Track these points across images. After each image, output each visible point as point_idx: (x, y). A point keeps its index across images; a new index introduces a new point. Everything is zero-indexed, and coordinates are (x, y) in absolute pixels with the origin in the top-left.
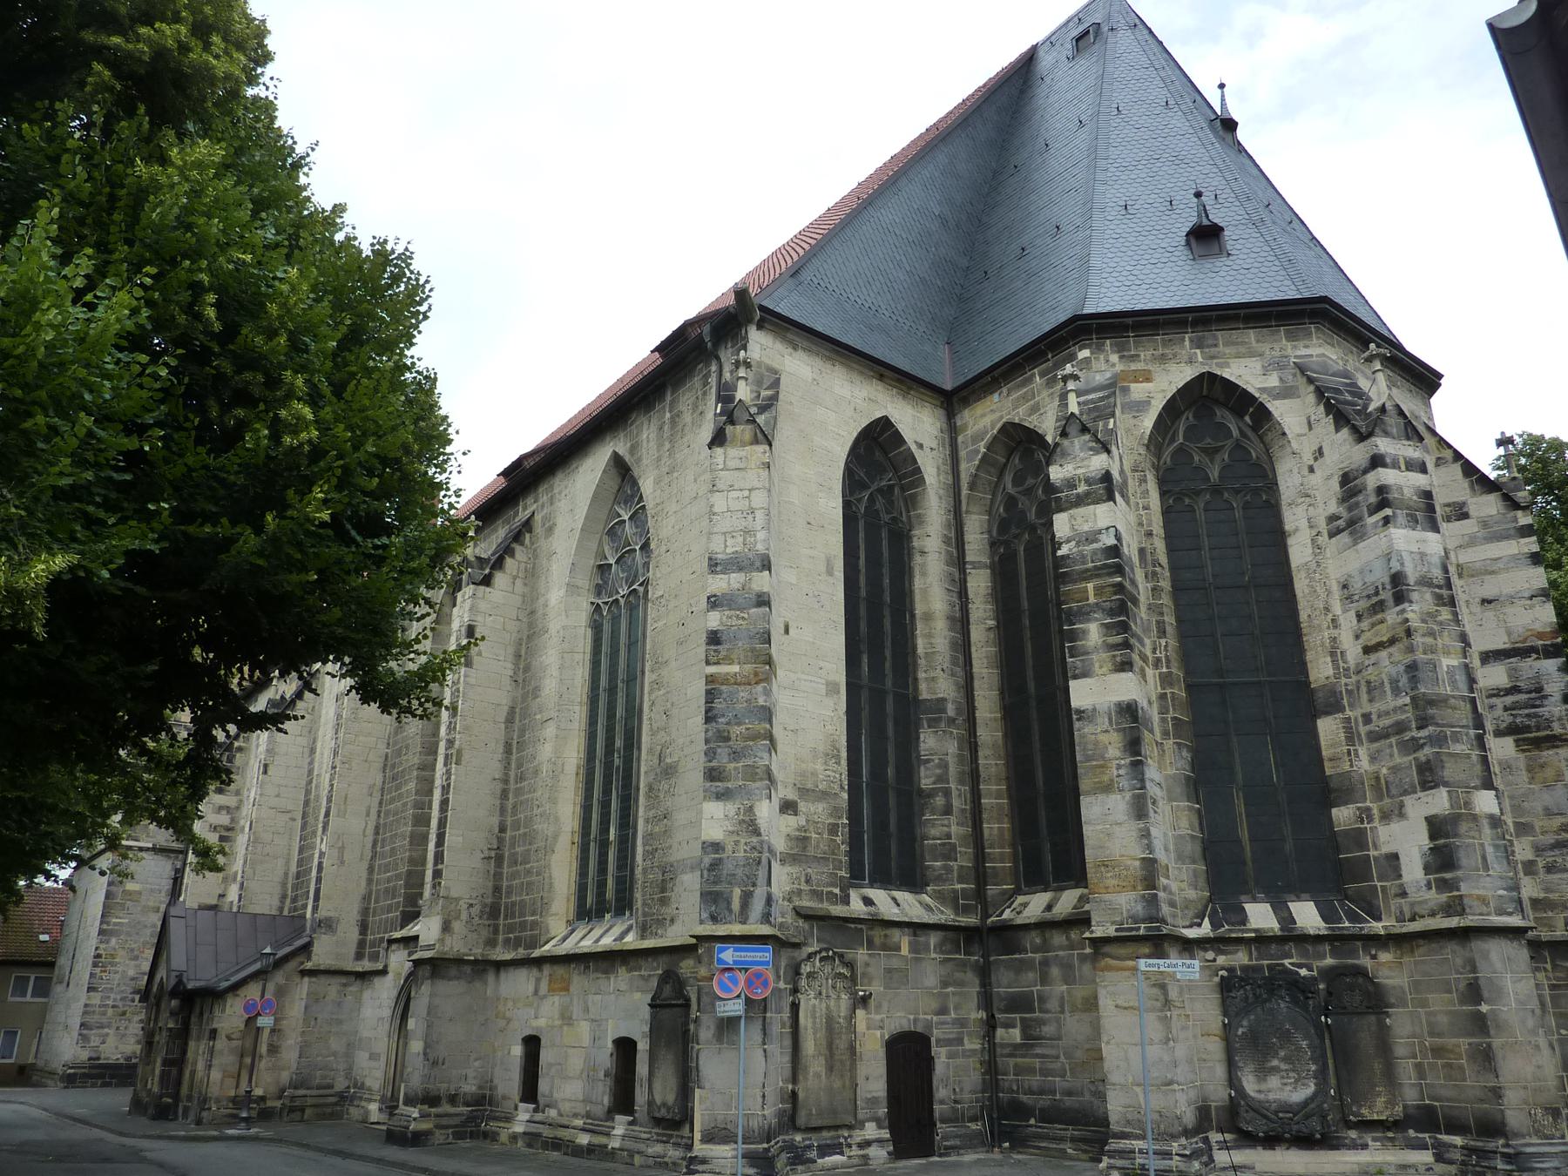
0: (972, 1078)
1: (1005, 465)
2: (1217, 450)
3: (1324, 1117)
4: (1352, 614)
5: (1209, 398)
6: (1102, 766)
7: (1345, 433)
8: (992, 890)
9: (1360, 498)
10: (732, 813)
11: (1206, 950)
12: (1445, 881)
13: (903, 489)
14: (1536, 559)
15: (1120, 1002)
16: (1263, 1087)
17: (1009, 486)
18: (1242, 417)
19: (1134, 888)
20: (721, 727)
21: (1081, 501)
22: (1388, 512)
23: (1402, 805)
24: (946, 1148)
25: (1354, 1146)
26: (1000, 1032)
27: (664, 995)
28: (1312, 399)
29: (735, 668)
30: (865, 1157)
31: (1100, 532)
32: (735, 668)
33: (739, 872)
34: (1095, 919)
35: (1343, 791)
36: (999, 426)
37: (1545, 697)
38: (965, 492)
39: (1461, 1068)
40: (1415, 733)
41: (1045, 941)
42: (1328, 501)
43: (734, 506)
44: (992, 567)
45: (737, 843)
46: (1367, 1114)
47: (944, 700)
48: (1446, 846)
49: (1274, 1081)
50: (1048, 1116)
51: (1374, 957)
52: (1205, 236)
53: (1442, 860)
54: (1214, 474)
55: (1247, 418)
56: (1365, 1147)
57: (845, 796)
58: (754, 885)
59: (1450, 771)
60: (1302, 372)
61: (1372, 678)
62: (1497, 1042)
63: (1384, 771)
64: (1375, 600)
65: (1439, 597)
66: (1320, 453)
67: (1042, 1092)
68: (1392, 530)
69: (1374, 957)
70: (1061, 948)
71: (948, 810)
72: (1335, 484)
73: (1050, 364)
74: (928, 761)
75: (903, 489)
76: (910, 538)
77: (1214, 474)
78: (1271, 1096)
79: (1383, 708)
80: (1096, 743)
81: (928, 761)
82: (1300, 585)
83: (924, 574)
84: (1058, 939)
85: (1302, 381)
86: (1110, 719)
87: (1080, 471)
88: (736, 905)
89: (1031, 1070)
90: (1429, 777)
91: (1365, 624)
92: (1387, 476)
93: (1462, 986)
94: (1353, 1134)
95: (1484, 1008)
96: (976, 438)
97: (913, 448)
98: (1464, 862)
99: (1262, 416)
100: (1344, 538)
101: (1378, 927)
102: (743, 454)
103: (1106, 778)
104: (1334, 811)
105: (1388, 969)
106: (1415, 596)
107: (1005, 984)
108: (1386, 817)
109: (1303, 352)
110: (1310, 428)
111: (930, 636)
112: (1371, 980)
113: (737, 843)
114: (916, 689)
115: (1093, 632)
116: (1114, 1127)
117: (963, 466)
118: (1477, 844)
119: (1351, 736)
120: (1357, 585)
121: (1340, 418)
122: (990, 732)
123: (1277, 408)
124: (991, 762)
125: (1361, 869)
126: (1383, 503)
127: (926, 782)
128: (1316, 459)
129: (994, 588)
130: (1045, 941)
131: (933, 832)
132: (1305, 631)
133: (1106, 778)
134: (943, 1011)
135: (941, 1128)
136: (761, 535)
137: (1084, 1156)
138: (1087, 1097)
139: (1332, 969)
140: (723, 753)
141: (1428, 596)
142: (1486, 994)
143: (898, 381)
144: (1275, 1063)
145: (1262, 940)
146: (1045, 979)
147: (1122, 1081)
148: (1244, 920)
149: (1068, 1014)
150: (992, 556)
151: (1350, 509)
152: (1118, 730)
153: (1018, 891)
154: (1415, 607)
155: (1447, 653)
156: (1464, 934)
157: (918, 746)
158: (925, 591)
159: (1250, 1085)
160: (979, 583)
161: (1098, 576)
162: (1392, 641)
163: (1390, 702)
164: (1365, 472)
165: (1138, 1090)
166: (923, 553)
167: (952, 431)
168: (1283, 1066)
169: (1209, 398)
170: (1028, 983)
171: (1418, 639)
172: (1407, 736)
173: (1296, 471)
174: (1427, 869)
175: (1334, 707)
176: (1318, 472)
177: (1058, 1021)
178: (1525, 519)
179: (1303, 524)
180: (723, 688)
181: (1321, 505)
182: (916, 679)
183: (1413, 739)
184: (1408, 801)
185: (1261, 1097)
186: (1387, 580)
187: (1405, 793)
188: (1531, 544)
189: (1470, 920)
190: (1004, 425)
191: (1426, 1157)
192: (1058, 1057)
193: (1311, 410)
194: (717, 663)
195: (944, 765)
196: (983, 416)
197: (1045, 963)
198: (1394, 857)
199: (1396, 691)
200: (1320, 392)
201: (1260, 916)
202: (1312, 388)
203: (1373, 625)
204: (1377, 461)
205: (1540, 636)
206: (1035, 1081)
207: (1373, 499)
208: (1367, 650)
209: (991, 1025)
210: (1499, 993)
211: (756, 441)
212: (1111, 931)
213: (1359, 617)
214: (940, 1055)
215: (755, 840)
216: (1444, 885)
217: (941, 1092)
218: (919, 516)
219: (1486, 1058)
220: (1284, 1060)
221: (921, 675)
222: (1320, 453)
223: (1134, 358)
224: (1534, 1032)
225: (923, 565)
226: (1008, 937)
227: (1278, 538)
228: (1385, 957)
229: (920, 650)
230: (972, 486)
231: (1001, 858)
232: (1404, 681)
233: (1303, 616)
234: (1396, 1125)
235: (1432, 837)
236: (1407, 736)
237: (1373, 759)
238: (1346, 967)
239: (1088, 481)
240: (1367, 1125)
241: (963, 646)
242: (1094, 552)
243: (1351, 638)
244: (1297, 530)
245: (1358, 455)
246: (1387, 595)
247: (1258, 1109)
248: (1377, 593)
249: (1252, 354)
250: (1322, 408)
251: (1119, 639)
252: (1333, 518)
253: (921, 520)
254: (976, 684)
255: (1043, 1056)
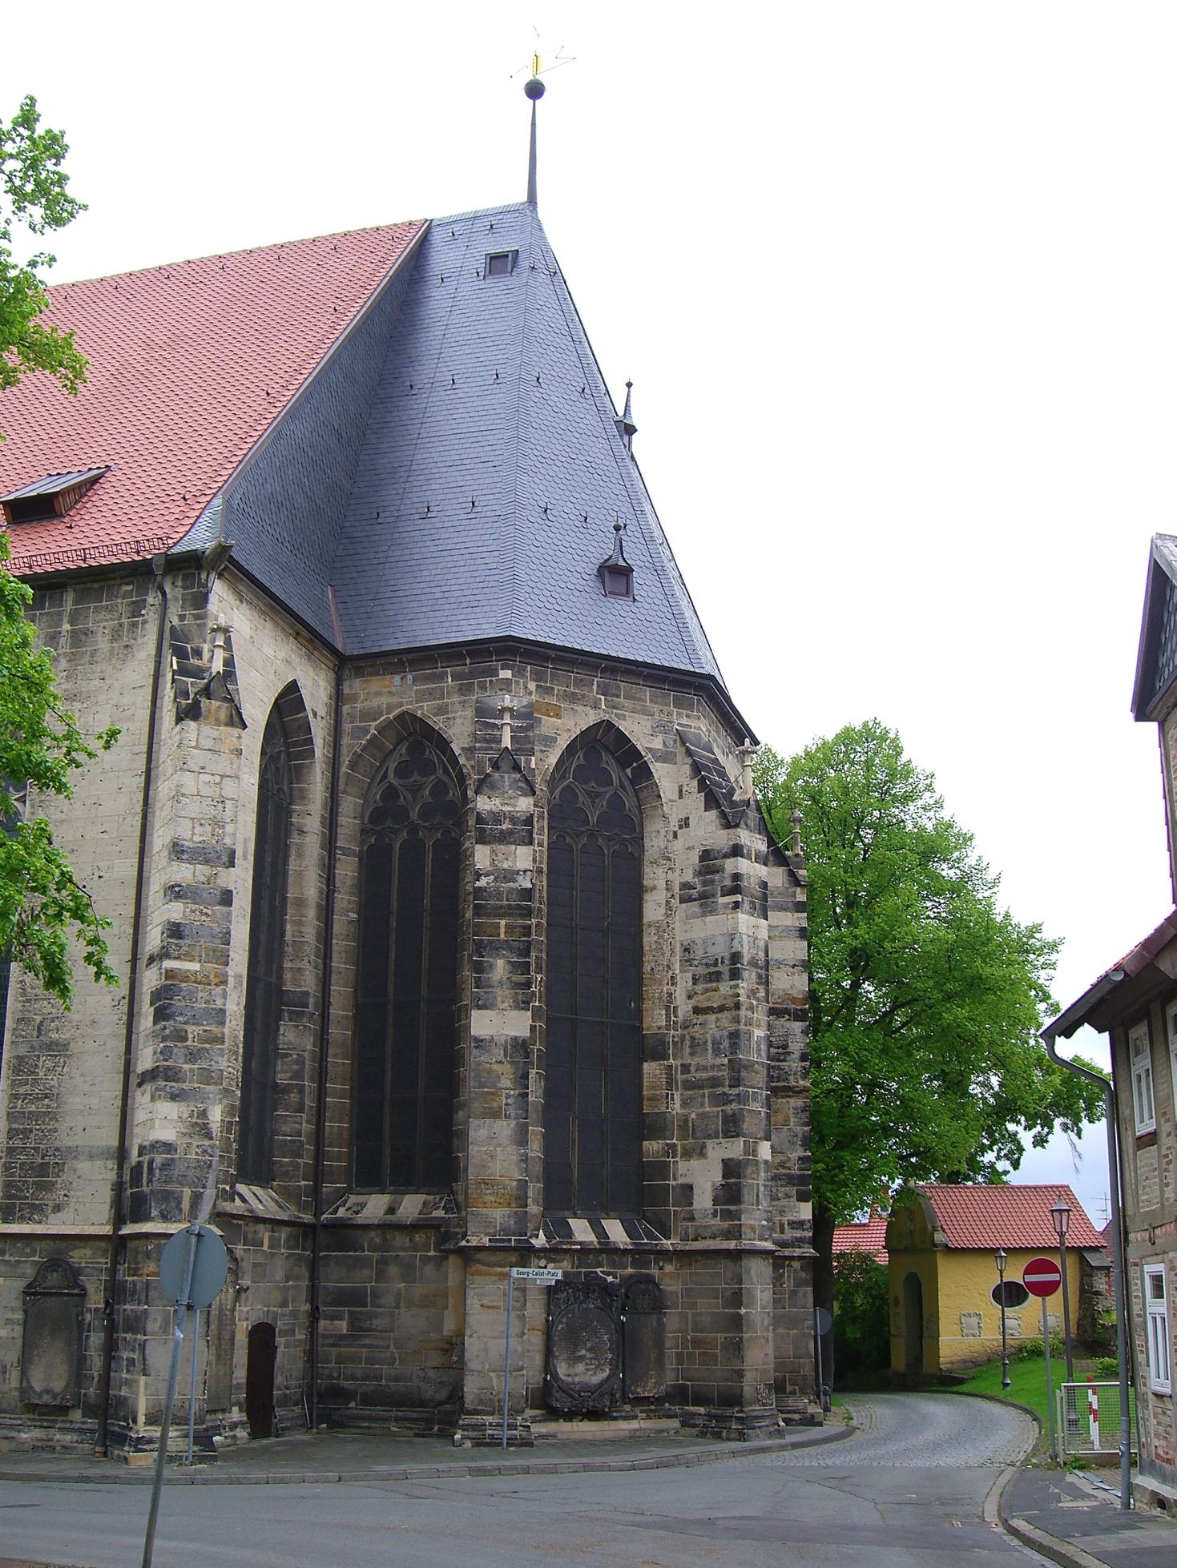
0: (298, 1366)
1: (391, 752)
2: (598, 795)
3: (613, 1395)
4: (690, 975)
5: (604, 746)
6: (493, 1094)
7: (713, 814)
8: (327, 1188)
9: (717, 877)
10: (186, 1115)
11: (540, 1258)
12: (730, 1211)
13: (290, 756)
14: (803, 933)
15: (484, 1302)
16: (572, 1371)
17: (391, 774)
18: (624, 769)
19: (509, 1205)
20: (178, 1026)
21: (504, 838)
22: (739, 898)
23: (704, 1146)
24: (283, 1429)
25: (627, 1418)
26: (323, 1324)
27: (48, 1283)
28: (687, 769)
29: (195, 966)
30: (234, 1437)
31: (518, 873)
32: (195, 966)
33: (190, 1173)
34: (471, 1228)
35: (655, 1127)
36: (396, 712)
37: (789, 1053)
38: (344, 769)
39: (715, 1355)
40: (726, 1090)
41: (385, 1240)
42: (686, 868)
43: (207, 791)
44: (360, 856)
45: (189, 1145)
46: (642, 1392)
47: (307, 993)
48: (736, 1184)
49: (580, 1367)
50: (368, 1400)
51: (661, 1268)
52: (615, 576)
53: (730, 1195)
54: (593, 819)
55: (629, 771)
56: (635, 1417)
57: (239, 1093)
58: (204, 1187)
59: (747, 1125)
60: (683, 743)
61: (697, 1035)
62: (746, 1336)
63: (693, 1116)
64: (712, 969)
65: (759, 976)
66: (685, 823)
67: (366, 1378)
68: (740, 915)
69: (661, 1268)
70: (403, 1249)
71: (300, 1109)
72: (694, 857)
73: (466, 669)
74: (286, 1055)
75: (290, 756)
76: (289, 813)
77: (593, 819)
78: (577, 1379)
79: (703, 1063)
80: (490, 1072)
81: (286, 1055)
82: (649, 939)
83: (300, 855)
84: (401, 1240)
85: (681, 750)
86: (505, 1051)
87: (506, 808)
88: (186, 1205)
89: (356, 1359)
90: (732, 1127)
91: (699, 988)
92: (744, 865)
93: (727, 1294)
94: (628, 1408)
95: (743, 1311)
96: (368, 715)
97: (311, 716)
98: (746, 1198)
99: (644, 772)
100: (694, 907)
101: (667, 1244)
102: (216, 734)
103: (495, 1105)
104: (645, 1143)
105: (670, 1278)
106: (746, 974)
107: (334, 1279)
108: (688, 1154)
109: (684, 721)
110: (681, 797)
111: (300, 923)
112: (657, 1286)
113: (189, 1145)
114: (280, 977)
115: (500, 968)
116: (468, 1406)
117: (346, 741)
118: (757, 1183)
119: (670, 1083)
120: (699, 953)
121: (712, 801)
122: (338, 1032)
123: (658, 770)
124: (338, 1061)
125: (660, 1195)
126: (736, 890)
127: (282, 1078)
128: (681, 827)
129: (360, 879)
130: (385, 1240)
131: (285, 1128)
132: (645, 982)
133: (495, 1105)
134: (284, 1304)
135: (279, 1412)
136: (229, 828)
137: (411, 1433)
138: (416, 1382)
139: (631, 1276)
140: (179, 1052)
141: (754, 975)
142: (745, 1301)
143: (311, 642)
144: (583, 1352)
145: (585, 1250)
146: (381, 1276)
147: (480, 1368)
148: (570, 1234)
149: (403, 1310)
150: (363, 842)
151: (705, 883)
152: (512, 1063)
153: (349, 1190)
154: (744, 984)
155: (758, 1026)
156: (737, 1255)
157: (276, 1038)
158: (300, 874)
159: (562, 1369)
160: (347, 870)
161: (510, 915)
162: (722, 1009)
163: (710, 1059)
164: (725, 856)
165: (492, 1374)
166: (302, 832)
167: (338, 698)
168: (588, 1355)
169: (604, 746)
170: (363, 1280)
171: (743, 1012)
172: (720, 1090)
173: (663, 833)
174: (715, 1201)
175: (661, 1055)
176: (680, 840)
177: (392, 1315)
178: (801, 897)
179: (662, 884)
180: (183, 985)
181: (678, 872)
182: (281, 968)
183: (724, 1093)
184: (710, 1144)
185: (570, 1379)
186: (727, 955)
187: (709, 1137)
188: (800, 920)
189: (745, 1244)
190: (403, 714)
191: (675, 1423)
192: (388, 1347)
193: (685, 781)
194: (178, 958)
195: (301, 1061)
196: (379, 694)
197: (383, 1261)
198: (689, 1188)
199: (717, 1052)
200: (697, 768)
201: (581, 1230)
202: (689, 760)
203: (707, 991)
204: (737, 851)
205: (794, 1000)
206: (360, 1368)
207: (728, 882)
208: (697, 1011)
209: (314, 1316)
210: (751, 1304)
211: (231, 723)
212: (486, 1241)
213: (695, 980)
214: (280, 1341)
215: (207, 1143)
216: (728, 1215)
217: (279, 1380)
218: (301, 790)
219: (737, 1348)
220: (588, 1350)
221: (287, 965)
222: (685, 823)
223: (549, 691)
224: (767, 1330)
225: (300, 846)
226: (343, 1234)
227: (636, 891)
228: (669, 1268)
229: (288, 937)
230: (353, 766)
231: (338, 1157)
232: (726, 1044)
233: (647, 968)
234: (659, 1400)
235: (724, 1177)
236: (720, 1090)
237: (685, 1104)
238: (640, 1275)
239: (513, 820)
240: (639, 1401)
241: (326, 936)
242: (511, 891)
243: (684, 996)
244: (654, 888)
245: (721, 839)
246: (724, 969)
247: (566, 1389)
248: (716, 965)
249: (645, 712)
250: (695, 783)
251: (522, 978)
252: (685, 886)
253: (303, 796)
254: (334, 978)
255: (370, 1346)
